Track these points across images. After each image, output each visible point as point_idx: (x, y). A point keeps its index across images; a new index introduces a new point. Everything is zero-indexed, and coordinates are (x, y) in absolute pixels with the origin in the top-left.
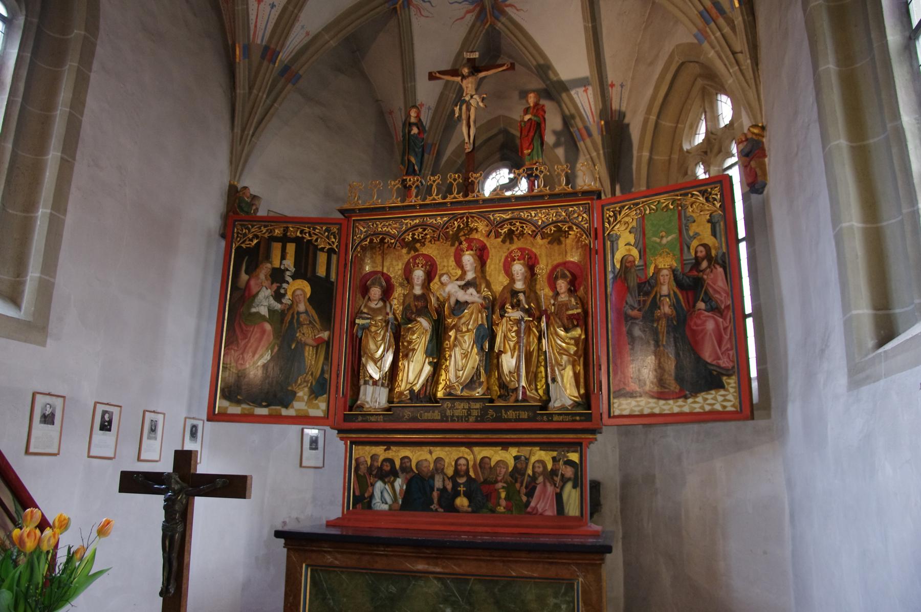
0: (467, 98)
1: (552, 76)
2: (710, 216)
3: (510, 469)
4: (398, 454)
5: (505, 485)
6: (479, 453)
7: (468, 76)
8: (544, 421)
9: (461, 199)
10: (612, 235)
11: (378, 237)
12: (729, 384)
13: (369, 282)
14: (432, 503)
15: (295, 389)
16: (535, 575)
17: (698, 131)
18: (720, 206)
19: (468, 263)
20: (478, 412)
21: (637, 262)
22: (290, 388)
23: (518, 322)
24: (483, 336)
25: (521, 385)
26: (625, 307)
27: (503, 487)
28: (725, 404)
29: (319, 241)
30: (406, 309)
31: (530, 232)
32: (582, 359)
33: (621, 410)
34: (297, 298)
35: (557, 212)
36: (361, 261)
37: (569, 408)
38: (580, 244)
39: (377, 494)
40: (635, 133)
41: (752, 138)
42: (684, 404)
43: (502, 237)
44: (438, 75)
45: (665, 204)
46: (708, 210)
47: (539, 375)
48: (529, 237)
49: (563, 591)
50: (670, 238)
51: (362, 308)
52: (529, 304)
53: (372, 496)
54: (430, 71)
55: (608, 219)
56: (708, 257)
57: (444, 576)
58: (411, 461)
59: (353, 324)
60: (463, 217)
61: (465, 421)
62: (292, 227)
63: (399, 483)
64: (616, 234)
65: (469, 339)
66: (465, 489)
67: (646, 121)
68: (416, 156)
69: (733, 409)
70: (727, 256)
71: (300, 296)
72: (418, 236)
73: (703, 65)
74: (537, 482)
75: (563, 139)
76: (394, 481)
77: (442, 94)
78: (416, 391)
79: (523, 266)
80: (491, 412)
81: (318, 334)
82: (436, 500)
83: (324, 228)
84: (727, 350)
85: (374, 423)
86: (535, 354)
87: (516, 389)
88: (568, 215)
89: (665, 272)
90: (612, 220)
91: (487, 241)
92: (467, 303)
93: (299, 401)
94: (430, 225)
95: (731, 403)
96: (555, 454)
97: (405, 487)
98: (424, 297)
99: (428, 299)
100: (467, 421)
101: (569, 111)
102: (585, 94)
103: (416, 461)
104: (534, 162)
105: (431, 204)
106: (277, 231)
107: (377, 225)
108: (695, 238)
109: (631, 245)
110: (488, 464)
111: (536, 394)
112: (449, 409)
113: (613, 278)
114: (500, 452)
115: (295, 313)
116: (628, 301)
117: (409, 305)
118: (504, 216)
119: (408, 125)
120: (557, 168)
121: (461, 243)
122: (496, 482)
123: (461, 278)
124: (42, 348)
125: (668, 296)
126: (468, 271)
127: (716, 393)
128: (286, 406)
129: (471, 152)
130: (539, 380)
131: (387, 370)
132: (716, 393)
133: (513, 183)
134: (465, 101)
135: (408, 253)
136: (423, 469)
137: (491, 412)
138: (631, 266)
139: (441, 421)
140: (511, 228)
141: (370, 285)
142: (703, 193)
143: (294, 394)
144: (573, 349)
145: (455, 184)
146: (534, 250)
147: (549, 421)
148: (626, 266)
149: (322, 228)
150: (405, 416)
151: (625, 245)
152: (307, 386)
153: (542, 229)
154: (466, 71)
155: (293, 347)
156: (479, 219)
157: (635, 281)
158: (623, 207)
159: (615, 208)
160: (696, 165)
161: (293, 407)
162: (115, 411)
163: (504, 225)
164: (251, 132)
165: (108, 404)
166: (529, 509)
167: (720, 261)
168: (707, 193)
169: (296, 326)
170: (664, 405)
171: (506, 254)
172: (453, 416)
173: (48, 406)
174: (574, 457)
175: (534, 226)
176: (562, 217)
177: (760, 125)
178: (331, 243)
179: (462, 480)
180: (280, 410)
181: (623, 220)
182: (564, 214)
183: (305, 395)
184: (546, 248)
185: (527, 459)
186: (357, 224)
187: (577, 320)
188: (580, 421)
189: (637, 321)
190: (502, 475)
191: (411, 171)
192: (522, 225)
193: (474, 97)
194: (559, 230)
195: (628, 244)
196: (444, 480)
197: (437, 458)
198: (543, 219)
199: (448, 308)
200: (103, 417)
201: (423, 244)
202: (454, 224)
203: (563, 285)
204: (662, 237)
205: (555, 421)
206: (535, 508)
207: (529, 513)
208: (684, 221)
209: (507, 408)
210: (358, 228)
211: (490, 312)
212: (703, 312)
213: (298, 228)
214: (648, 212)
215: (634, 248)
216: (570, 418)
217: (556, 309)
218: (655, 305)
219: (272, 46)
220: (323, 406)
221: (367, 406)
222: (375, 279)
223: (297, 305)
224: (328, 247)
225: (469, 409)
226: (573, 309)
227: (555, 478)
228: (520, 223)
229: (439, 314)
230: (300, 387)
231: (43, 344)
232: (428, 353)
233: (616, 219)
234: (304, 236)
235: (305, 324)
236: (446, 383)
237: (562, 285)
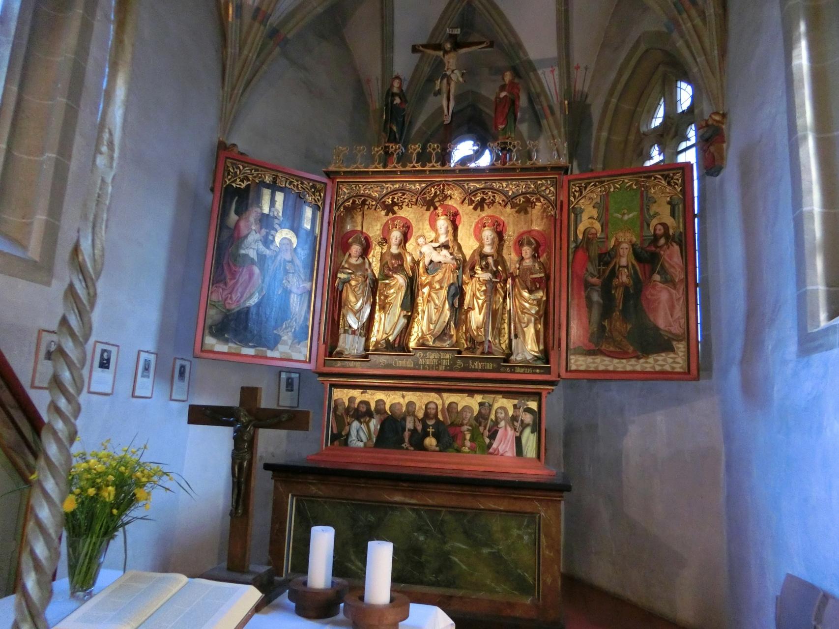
0: (448, 73)
1: (521, 54)
2: (670, 198)
3: (475, 414)
4: (373, 397)
5: (470, 428)
6: (447, 398)
7: (450, 52)
8: (507, 373)
12: (678, 348)
13: (350, 240)
14: (403, 442)
16: (502, 508)
17: (656, 115)
18: (681, 190)
21: (598, 235)
23: (486, 282)
27: (468, 430)
28: (675, 365)
30: (384, 265)
31: (501, 202)
32: (542, 319)
33: (577, 365)
35: (526, 185)
37: (531, 361)
38: (545, 214)
39: (353, 433)
40: (596, 112)
41: (712, 125)
42: (636, 363)
43: (474, 204)
44: (421, 48)
45: (628, 184)
46: (669, 193)
47: (503, 331)
48: (498, 206)
49: (525, 523)
50: (631, 215)
51: (343, 263)
52: (497, 267)
53: (348, 434)
54: (413, 44)
55: (574, 194)
56: (666, 234)
57: (418, 507)
58: (385, 403)
60: (440, 185)
61: (436, 369)
63: (374, 424)
64: (581, 208)
66: (433, 430)
67: (607, 103)
68: (397, 126)
69: (681, 370)
70: (683, 235)
73: (666, 53)
74: (499, 426)
75: (527, 116)
76: (369, 421)
77: (417, 66)
80: (459, 362)
82: (407, 440)
83: (311, 184)
84: (678, 318)
86: (500, 311)
87: (482, 343)
88: (537, 187)
89: (625, 245)
90: (577, 194)
91: (460, 207)
94: (410, 191)
95: (680, 365)
96: (516, 402)
97: (379, 427)
98: (399, 257)
100: (437, 370)
101: (535, 90)
102: (551, 75)
103: (390, 404)
104: (507, 136)
105: (411, 171)
108: (654, 217)
109: (594, 219)
110: (455, 409)
111: (499, 347)
112: (421, 358)
113: (574, 247)
114: (467, 398)
116: (589, 270)
118: (478, 186)
119: (390, 95)
120: (529, 143)
121: (436, 208)
122: (462, 425)
123: (436, 240)
124: (47, 288)
125: (627, 267)
127: (666, 356)
129: (448, 124)
131: (364, 321)
132: (666, 356)
133: (478, 154)
134: (445, 76)
135: (387, 214)
136: (397, 411)
138: (593, 238)
139: (414, 369)
140: (483, 197)
142: (665, 177)
145: (434, 153)
146: (502, 218)
147: (511, 372)
152: (291, 331)
153: (512, 199)
154: (448, 46)
156: (454, 187)
158: (590, 183)
160: (651, 148)
161: (278, 350)
162: (114, 350)
163: (477, 194)
164: (240, 91)
165: (106, 343)
166: (491, 450)
167: (677, 240)
168: (669, 178)
170: (618, 363)
171: (477, 220)
173: (53, 343)
174: (533, 405)
175: (505, 196)
176: (531, 189)
177: (721, 112)
178: (316, 199)
179: (431, 422)
180: (266, 352)
182: (533, 186)
184: (514, 216)
185: (491, 406)
186: (341, 186)
188: (540, 373)
190: (468, 419)
191: (392, 139)
193: (455, 72)
194: (528, 201)
195: (591, 218)
196: (415, 422)
197: (408, 403)
199: (423, 267)
200: (102, 355)
201: (401, 208)
202: (431, 190)
203: (528, 251)
204: (624, 214)
205: (518, 373)
206: (497, 449)
207: (491, 454)
208: (645, 201)
209: (474, 359)
212: (659, 283)
213: (287, 179)
214: (612, 190)
215: (597, 222)
216: (530, 370)
218: (613, 274)
219: (264, 8)
225: (440, 359)
226: (536, 274)
227: (516, 423)
228: (492, 192)
229: (413, 272)
230: (285, 331)
231: (48, 284)
232: (403, 306)
233: (581, 193)
236: (418, 335)
237: (527, 251)
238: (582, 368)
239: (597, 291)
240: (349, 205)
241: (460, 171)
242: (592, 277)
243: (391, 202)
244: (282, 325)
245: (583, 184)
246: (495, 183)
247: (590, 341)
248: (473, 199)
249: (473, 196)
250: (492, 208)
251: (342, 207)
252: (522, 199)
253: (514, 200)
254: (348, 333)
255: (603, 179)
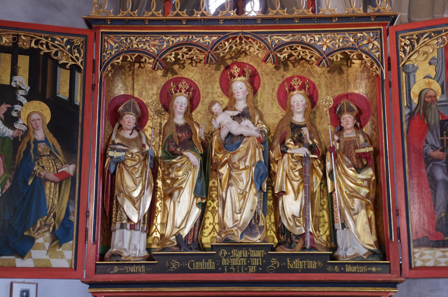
8: (336, 272)
9: (161, 17)
10: (408, 66)
11: (134, 55)
13: (121, 108)
15: (33, 234)
19: (240, 91)
20: (259, 262)
21: (438, 98)
22: (26, 233)
23: (301, 159)
24: (263, 174)
25: (308, 231)
26: (424, 147)
29: (59, 55)
33: (423, 261)
34: (33, 123)
36: (111, 82)
37: (365, 257)
51: (113, 137)
52: (312, 139)
55: (403, 48)
59: (104, 156)
61: (245, 271)
62: (24, 36)
64: (413, 65)
65: (247, 178)
71: (37, 121)
72: (183, 56)
78: (184, 237)
79: (304, 96)
80: (274, 261)
81: (62, 168)
83: (65, 40)
85: (134, 275)
87: (303, 236)
88: (357, 40)
90: (408, 49)
92: (242, 136)
93: (39, 249)
99: (192, 130)
100: (247, 271)
106: (4, 39)
107: (132, 41)
109: (431, 78)
112: (225, 258)
115: (32, 141)
116: (429, 141)
117: (172, 136)
126: (240, 100)
128: (22, 256)
130: (321, 225)
135: (165, 75)
137: (274, 261)
141: (123, 111)
143: (32, 240)
144: (364, 191)
147: (341, 272)
148: (425, 101)
149: (63, 39)
150: (172, 266)
151: (424, 78)
153: (327, 56)
155: (30, 183)
156: (254, 40)
157: (437, 118)
158: (422, 35)
159: (412, 35)
161: (30, 257)
163: (284, 49)
169: (33, 158)
171: (280, 82)
172: (230, 266)
176: (350, 43)
178: (74, 58)
180: (14, 261)
181: (420, 50)
182: (352, 40)
183: (46, 241)
184: (326, 77)
186: (106, 38)
187: (367, 159)
188: (376, 272)
189: (440, 163)
192: (304, 50)
195: (427, 77)
198: (328, 44)
202: (225, 45)
205: (349, 272)
209: (293, 257)
210: (108, 42)
211: (267, 147)
213: (32, 37)
215: (435, 82)
216: (364, 268)
217: (343, 147)
220: (69, 254)
221: (125, 254)
222: (129, 105)
223: (34, 132)
224: (71, 63)
225: (249, 258)
228: (302, 47)
232: (197, 193)
234: (40, 47)
235: (44, 156)
238: (430, 264)
239: (442, 166)
240: (118, 63)
241: (263, 20)
242: (434, 151)
243: (173, 60)
244: (36, 223)
245: (414, 36)
246: (305, 35)
247: (437, 230)
248: (279, 55)
249: (278, 52)
250: (298, 67)
251: (109, 65)
252: (339, 55)
253: (329, 57)
254: (127, 229)
255: (440, 29)
